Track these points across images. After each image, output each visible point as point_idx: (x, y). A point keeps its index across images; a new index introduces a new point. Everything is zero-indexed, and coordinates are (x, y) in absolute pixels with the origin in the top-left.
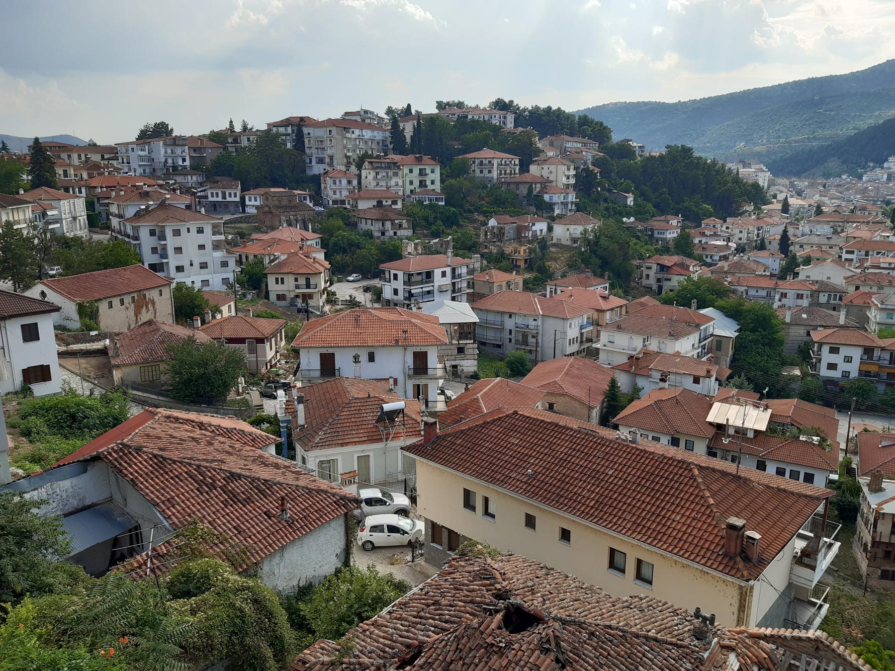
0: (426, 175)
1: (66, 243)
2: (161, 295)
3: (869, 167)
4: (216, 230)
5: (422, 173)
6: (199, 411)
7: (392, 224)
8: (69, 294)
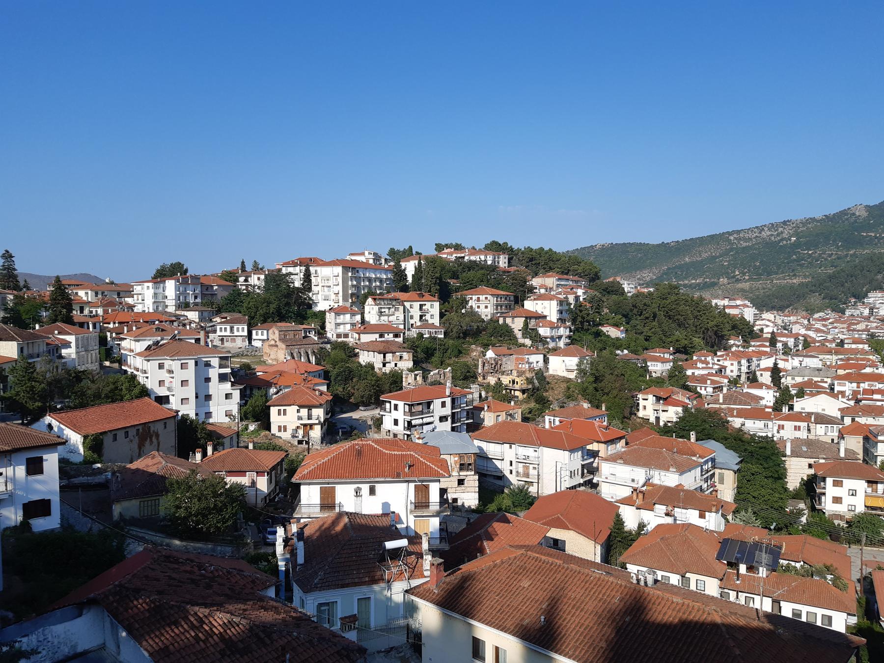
1: (78, 376)
4: (223, 362)
8: (75, 428)
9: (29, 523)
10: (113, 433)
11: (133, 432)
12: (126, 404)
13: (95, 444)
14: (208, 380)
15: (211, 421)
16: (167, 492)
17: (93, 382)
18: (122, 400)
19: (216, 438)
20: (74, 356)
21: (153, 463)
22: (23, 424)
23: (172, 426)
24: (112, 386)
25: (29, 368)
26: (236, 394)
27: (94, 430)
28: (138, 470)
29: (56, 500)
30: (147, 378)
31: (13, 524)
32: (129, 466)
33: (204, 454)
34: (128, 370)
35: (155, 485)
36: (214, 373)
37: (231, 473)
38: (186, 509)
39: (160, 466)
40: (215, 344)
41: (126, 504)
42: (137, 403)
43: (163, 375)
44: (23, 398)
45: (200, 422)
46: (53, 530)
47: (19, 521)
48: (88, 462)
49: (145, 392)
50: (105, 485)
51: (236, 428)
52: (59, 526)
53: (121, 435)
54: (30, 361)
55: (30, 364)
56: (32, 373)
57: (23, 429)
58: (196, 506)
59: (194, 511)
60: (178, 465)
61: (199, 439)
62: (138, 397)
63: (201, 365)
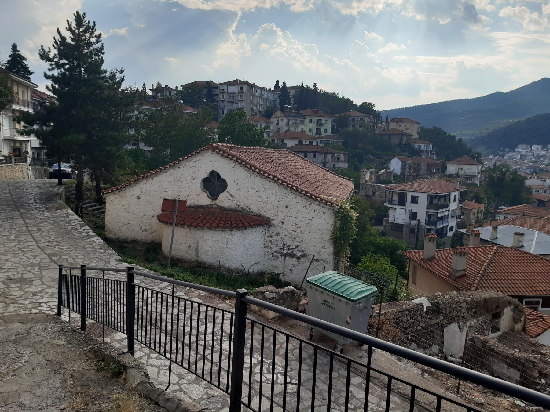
0: (322, 125)
3: (506, 151)
5: (319, 123)
6: (135, 294)
7: (332, 157)
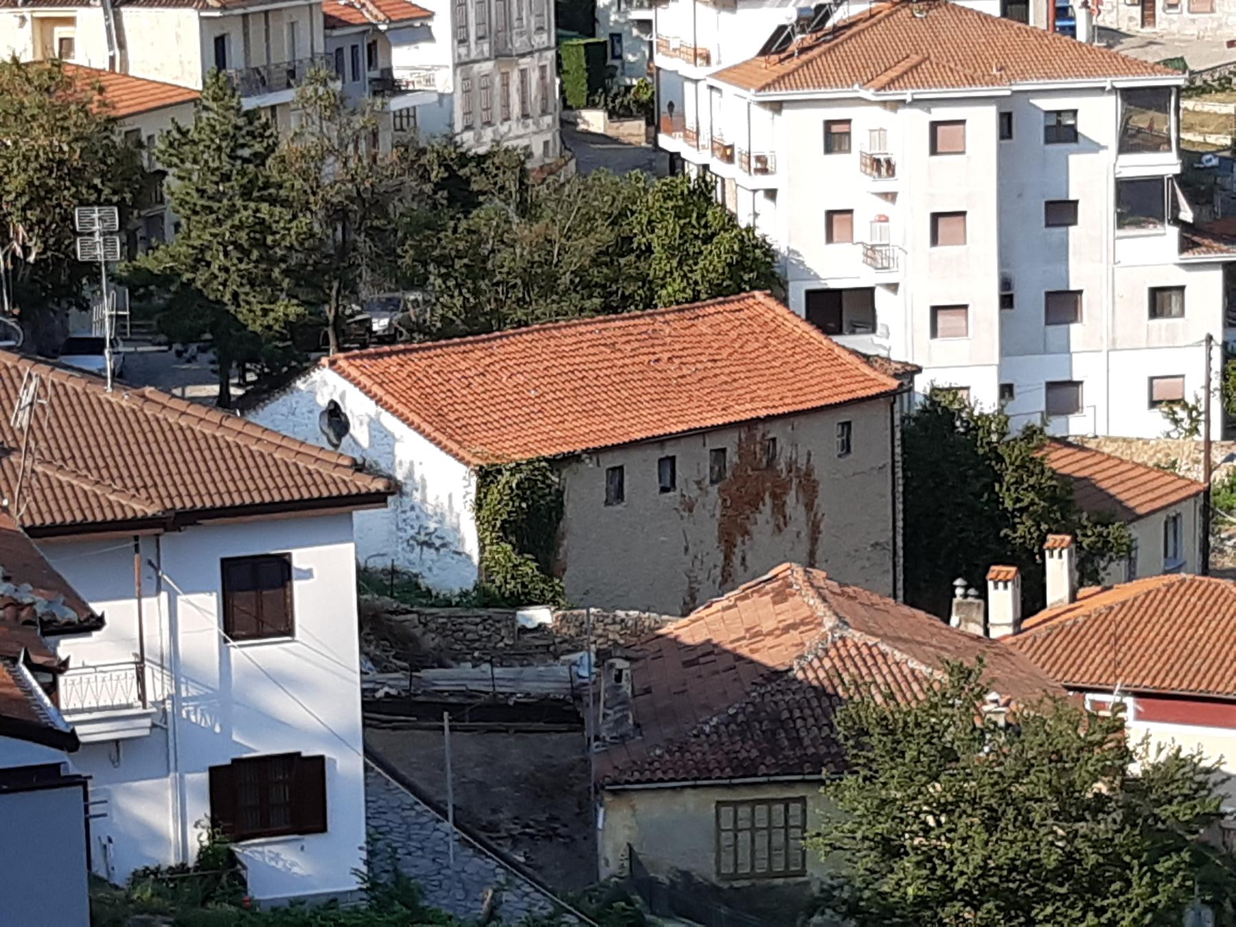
1: (458, 180)
2: (846, 447)
4: (1141, 120)
8: (443, 429)
9: (232, 859)
10: (610, 461)
11: (693, 465)
12: (666, 325)
13: (529, 512)
14: (1062, 212)
15: (1077, 426)
16: (843, 767)
17: (526, 209)
18: (649, 303)
19: (1095, 519)
20: (445, 81)
21: (779, 620)
22: (223, 401)
23: (877, 445)
24: (605, 235)
25: (243, 145)
26: (1206, 294)
27: (527, 443)
28: (710, 650)
29: (347, 767)
30: (771, 194)
31: (172, 860)
32: (674, 627)
33: (1032, 598)
34: (687, 152)
35: (780, 732)
36: (1092, 178)
37: (1158, 701)
38: (927, 859)
39: (812, 638)
40: (1106, 20)
41: (654, 808)
42: (715, 318)
43: (843, 179)
44: (222, 278)
45: (1016, 428)
46: (333, 901)
47: (194, 847)
48: (496, 599)
49: (756, 268)
50: (561, 712)
51: (1198, 474)
52: (354, 884)
53: (641, 474)
54: (248, 104)
55: (251, 115)
56: (260, 159)
57: (209, 424)
58: (972, 853)
59: (963, 874)
60: (895, 640)
61: (1007, 519)
62: (719, 292)
63: (1031, 132)
